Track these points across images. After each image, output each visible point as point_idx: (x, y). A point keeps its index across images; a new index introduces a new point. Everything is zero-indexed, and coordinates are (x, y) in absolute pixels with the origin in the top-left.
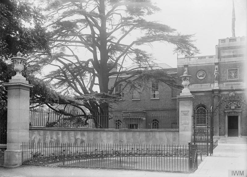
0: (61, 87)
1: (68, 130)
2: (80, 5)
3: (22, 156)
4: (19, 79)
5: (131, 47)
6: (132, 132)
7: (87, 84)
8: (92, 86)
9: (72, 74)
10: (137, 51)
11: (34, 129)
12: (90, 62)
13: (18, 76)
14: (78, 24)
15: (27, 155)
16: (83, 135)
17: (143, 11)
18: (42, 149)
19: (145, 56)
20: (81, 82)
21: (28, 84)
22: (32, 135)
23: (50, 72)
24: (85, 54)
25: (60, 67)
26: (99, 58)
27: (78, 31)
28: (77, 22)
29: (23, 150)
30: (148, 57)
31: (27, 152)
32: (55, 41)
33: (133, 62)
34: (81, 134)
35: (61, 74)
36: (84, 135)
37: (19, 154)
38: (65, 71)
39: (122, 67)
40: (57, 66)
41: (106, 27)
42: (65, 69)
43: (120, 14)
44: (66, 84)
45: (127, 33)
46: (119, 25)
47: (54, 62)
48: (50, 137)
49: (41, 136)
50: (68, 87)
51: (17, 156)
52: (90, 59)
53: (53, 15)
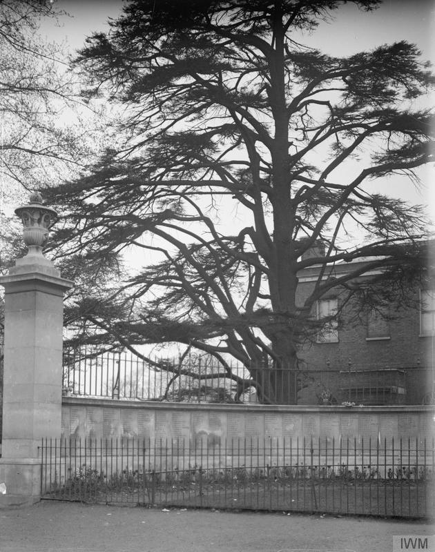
0: (172, 309)
1: (174, 409)
2: (214, 81)
3: (39, 476)
4: (33, 265)
5: (355, 189)
6: (357, 416)
7: (239, 299)
8: (251, 302)
9: (202, 274)
10: (376, 202)
11: (77, 405)
12: (248, 238)
13: (32, 258)
14: (215, 138)
15: (53, 474)
16: (214, 423)
17: (393, 88)
18: (99, 459)
19: (399, 212)
20: (223, 291)
21: (59, 277)
22: (71, 421)
23: (144, 268)
24: (232, 217)
25: (165, 252)
26: (270, 228)
27: (216, 156)
28: (212, 134)
29: (44, 459)
30: (407, 216)
31: (53, 466)
32: (156, 184)
33: (366, 233)
34: (210, 420)
35: (172, 273)
36: (218, 424)
37: (32, 471)
38: (183, 264)
39: (332, 246)
40: (158, 249)
41: (290, 140)
42: (183, 260)
43: (327, 103)
44: (187, 300)
45: (347, 152)
46: (322, 128)
47: (147, 237)
48: (121, 428)
49: (96, 422)
50: (192, 308)
51: (27, 475)
52: (246, 228)
53: (150, 117)
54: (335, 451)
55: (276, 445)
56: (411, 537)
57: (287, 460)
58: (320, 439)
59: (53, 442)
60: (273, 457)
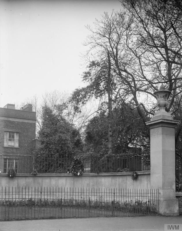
54: (25, 194)
55: (64, 190)
56: (172, 225)
57: (7, 196)
58: (70, 188)
59: (154, 191)
60: (5, 197)
